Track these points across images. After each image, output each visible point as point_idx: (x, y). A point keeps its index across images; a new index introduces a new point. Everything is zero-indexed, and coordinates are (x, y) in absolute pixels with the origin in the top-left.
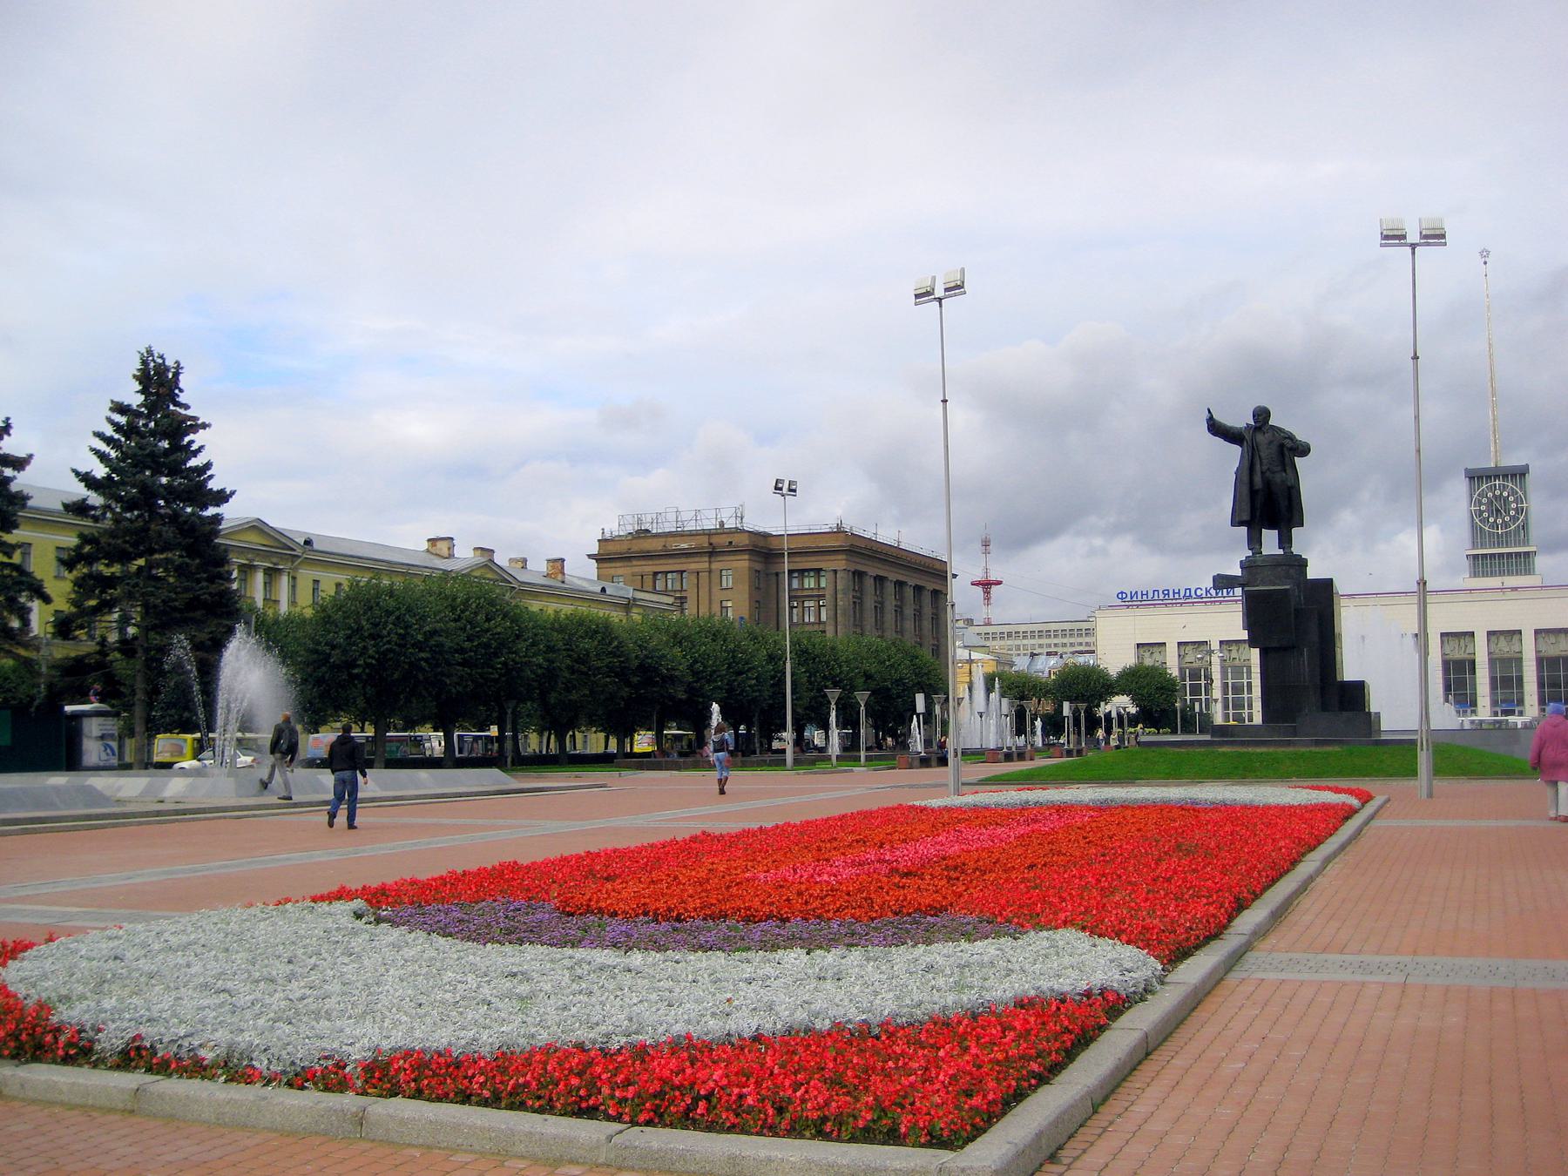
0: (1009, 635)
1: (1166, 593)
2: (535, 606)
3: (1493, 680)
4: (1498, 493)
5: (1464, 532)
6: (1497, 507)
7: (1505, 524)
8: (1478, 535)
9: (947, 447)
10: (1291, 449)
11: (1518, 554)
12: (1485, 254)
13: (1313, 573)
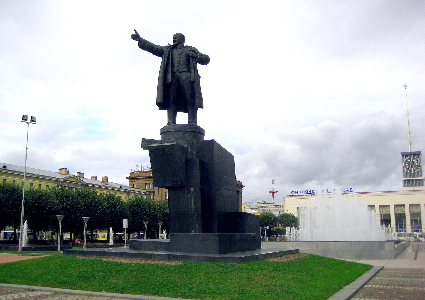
0: (276, 206)
1: (307, 191)
2: (99, 192)
3: (411, 221)
5: (401, 173)
6: (411, 165)
7: (414, 170)
8: (406, 174)
11: (418, 180)
12: (405, 86)
13: (206, 138)
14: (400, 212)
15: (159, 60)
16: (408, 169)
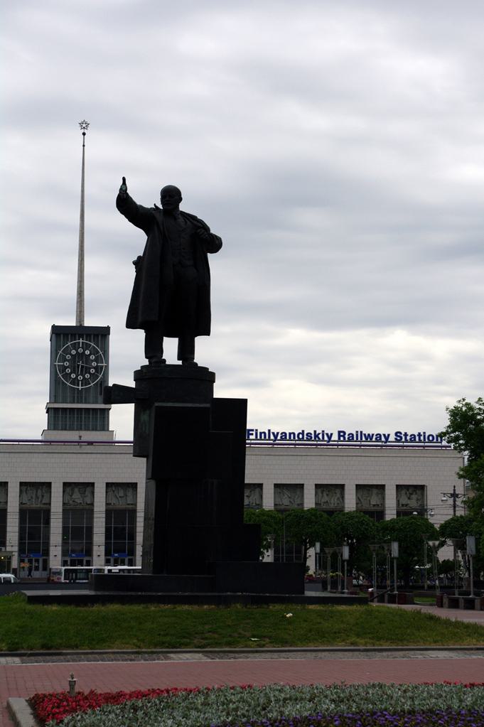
3: (65, 530)
4: (80, 350)
14: (35, 505)
16: (67, 376)
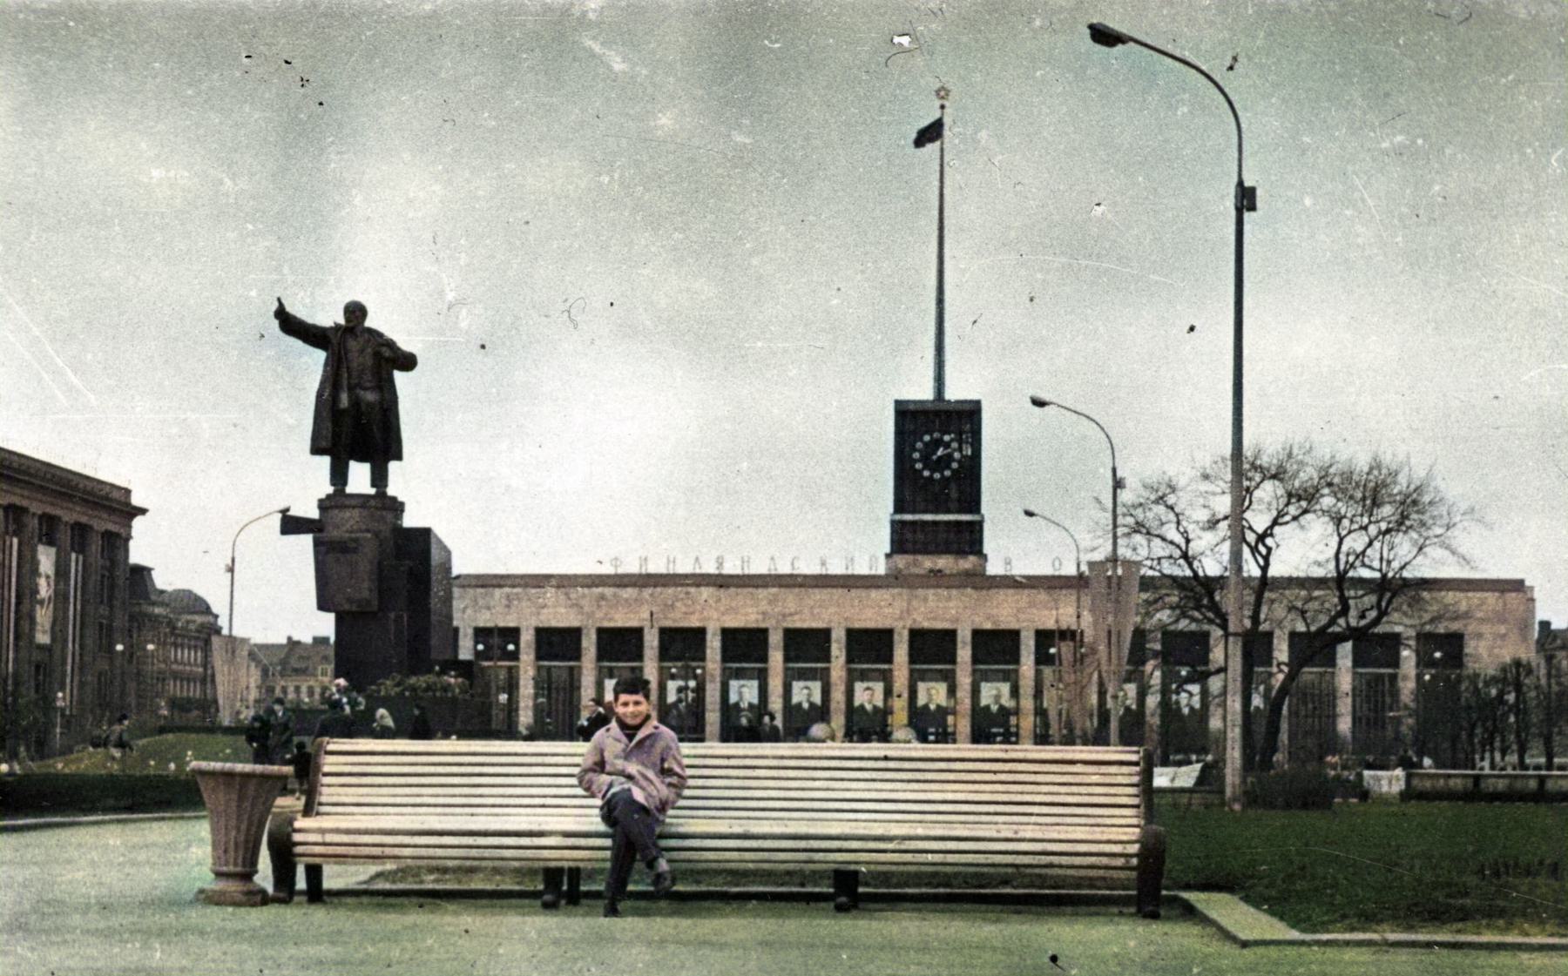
9: (940, 301)
10: (387, 360)
13: (410, 520)
15: (320, 356)
